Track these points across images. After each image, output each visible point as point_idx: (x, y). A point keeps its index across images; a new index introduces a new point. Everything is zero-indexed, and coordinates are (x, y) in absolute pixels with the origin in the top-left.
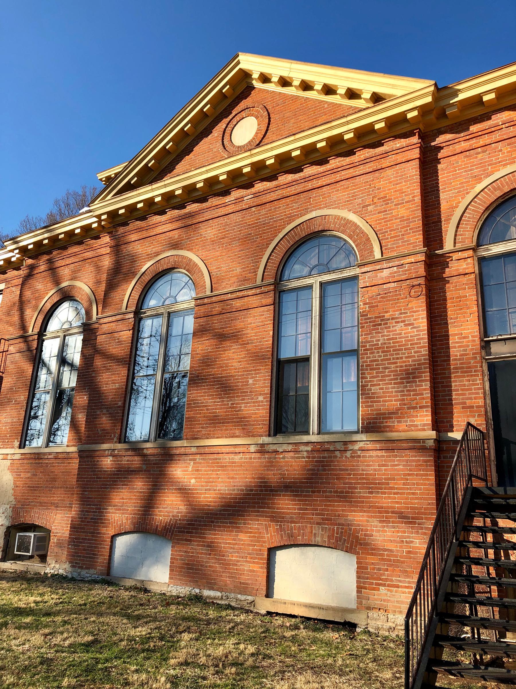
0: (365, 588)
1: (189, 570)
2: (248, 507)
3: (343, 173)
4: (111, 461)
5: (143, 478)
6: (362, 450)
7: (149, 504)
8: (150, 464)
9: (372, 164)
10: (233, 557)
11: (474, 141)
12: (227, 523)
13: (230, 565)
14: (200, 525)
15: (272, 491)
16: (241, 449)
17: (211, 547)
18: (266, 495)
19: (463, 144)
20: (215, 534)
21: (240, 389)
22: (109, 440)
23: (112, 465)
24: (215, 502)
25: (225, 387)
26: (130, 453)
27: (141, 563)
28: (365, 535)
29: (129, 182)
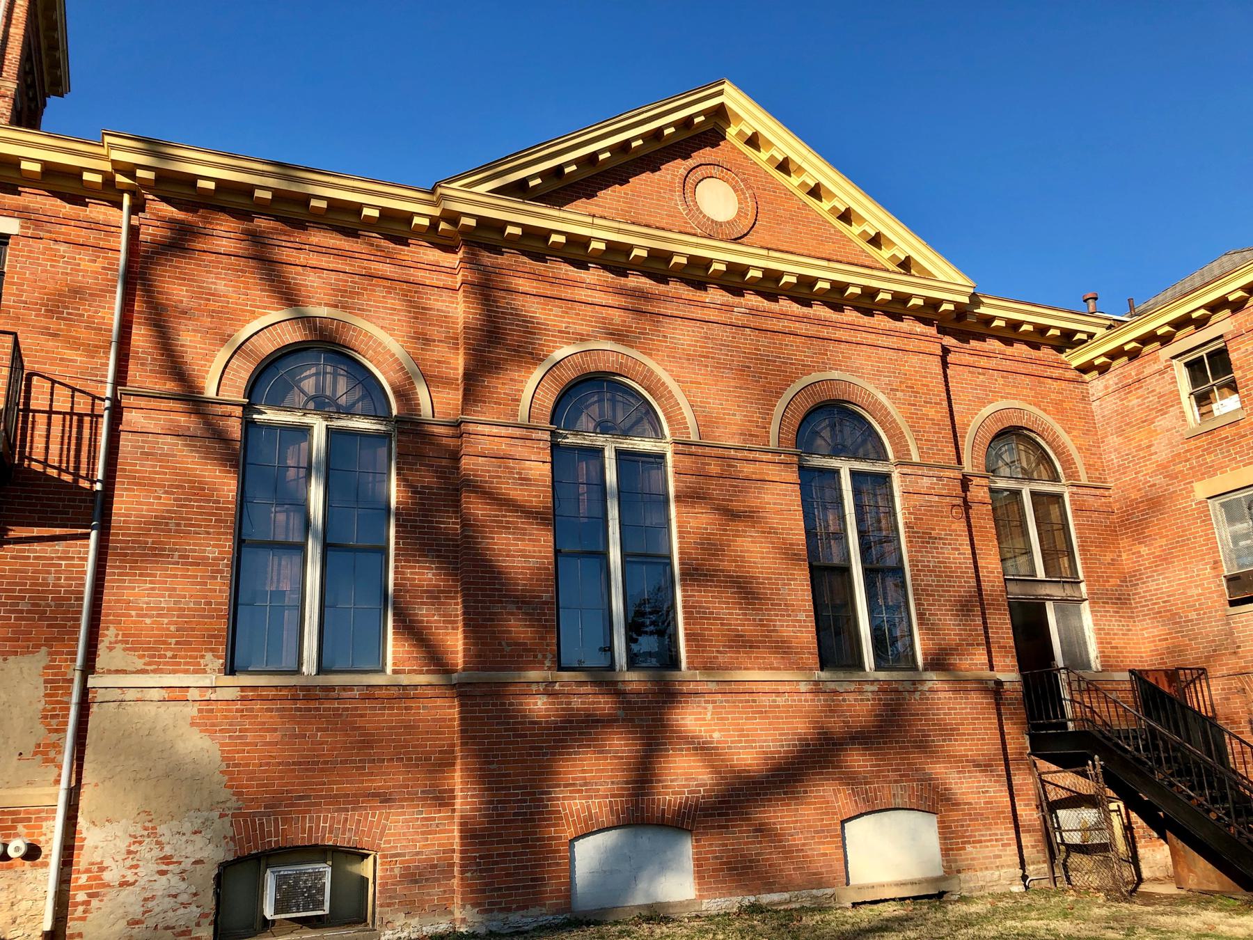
0: (952, 849)
1: (738, 871)
2: (807, 768)
3: (864, 335)
4: (544, 704)
5: (621, 733)
6: (931, 690)
7: (642, 777)
8: (633, 709)
9: (895, 339)
10: (799, 840)
11: (976, 358)
12: (779, 794)
13: (792, 851)
14: (739, 802)
15: (834, 744)
16: (787, 688)
17: (762, 830)
18: (829, 750)
19: (967, 357)
20: (765, 812)
21: (769, 599)
22: (537, 664)
23: (547, 710)
24: (758, 765)
25: (746, 591)
26: (588, 689)
27: (634, 878)
28: (946, 789)
29: (525, 181)
